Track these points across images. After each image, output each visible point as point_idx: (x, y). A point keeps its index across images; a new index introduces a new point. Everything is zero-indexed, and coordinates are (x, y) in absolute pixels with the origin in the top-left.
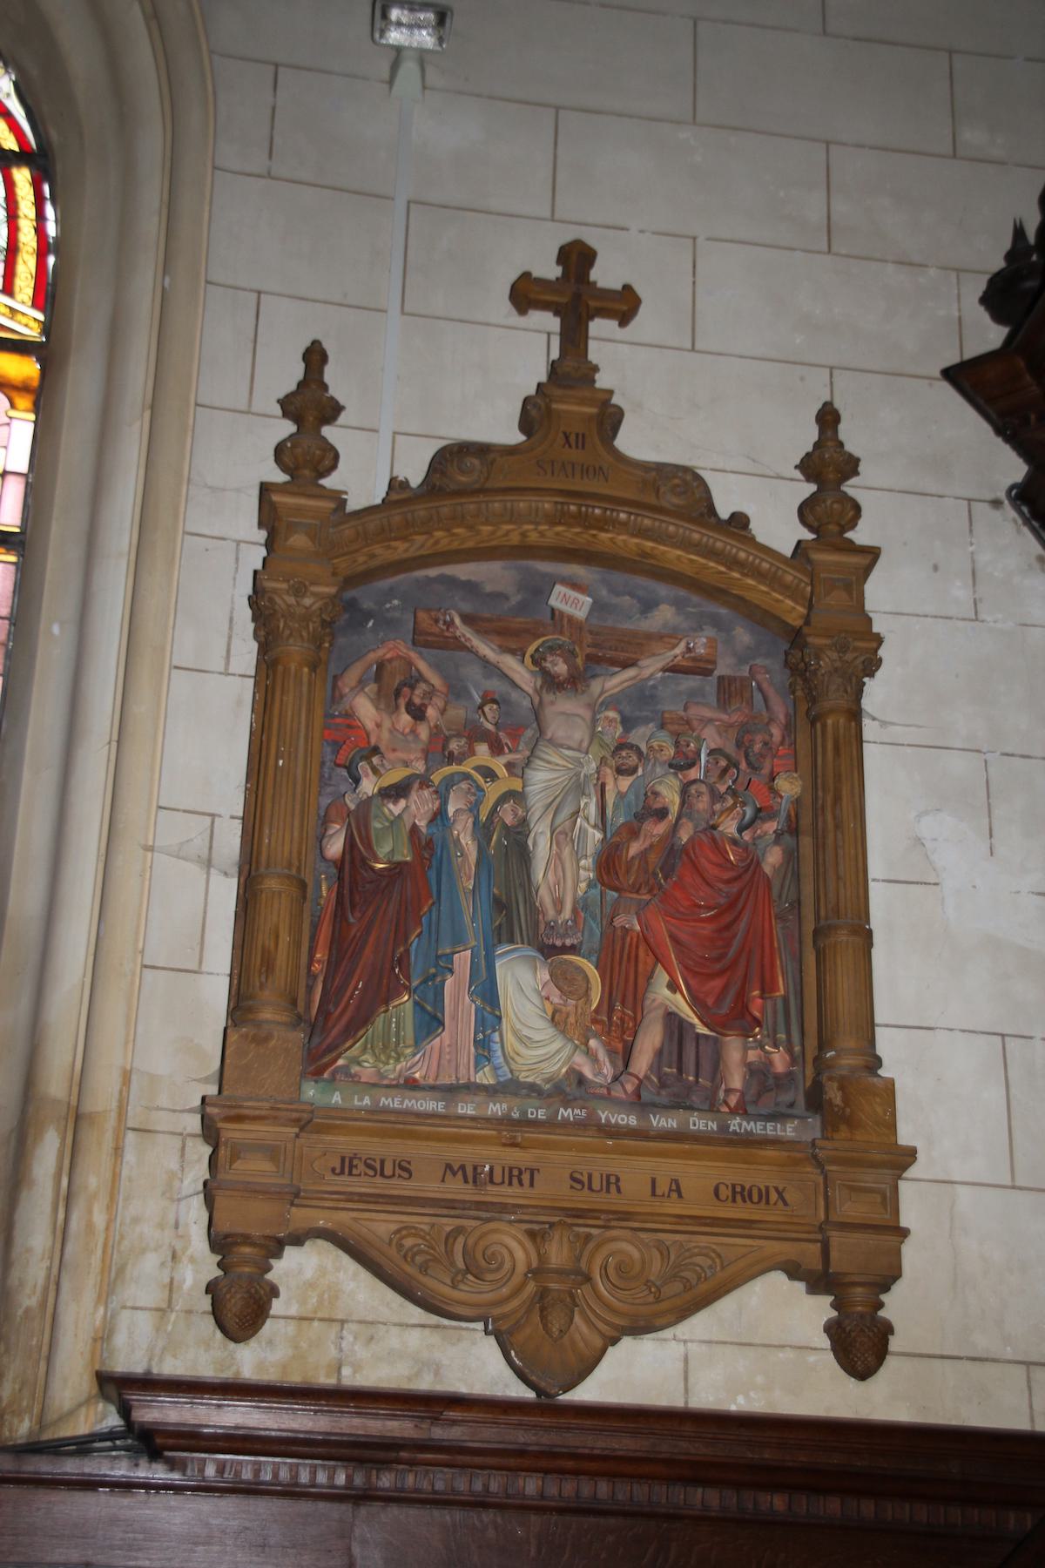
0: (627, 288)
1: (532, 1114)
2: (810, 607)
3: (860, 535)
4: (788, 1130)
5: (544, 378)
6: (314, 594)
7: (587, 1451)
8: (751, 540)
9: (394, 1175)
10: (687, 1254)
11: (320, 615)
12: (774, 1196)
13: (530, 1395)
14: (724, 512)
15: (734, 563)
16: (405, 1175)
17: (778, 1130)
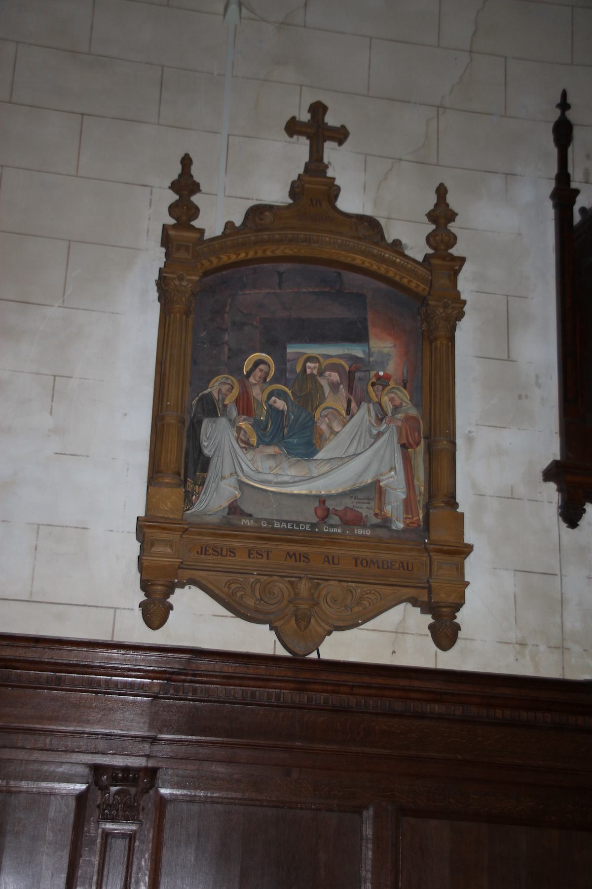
0: (343, 127)
1: (302, 527)
2: (431, 287)
3: (455, 251)
5: (301, 170)
9: (226, 556)
13: (287, 654)
14: (390, 240)
15: (394, 264)
16: (233, 555)
17: (295, 526)
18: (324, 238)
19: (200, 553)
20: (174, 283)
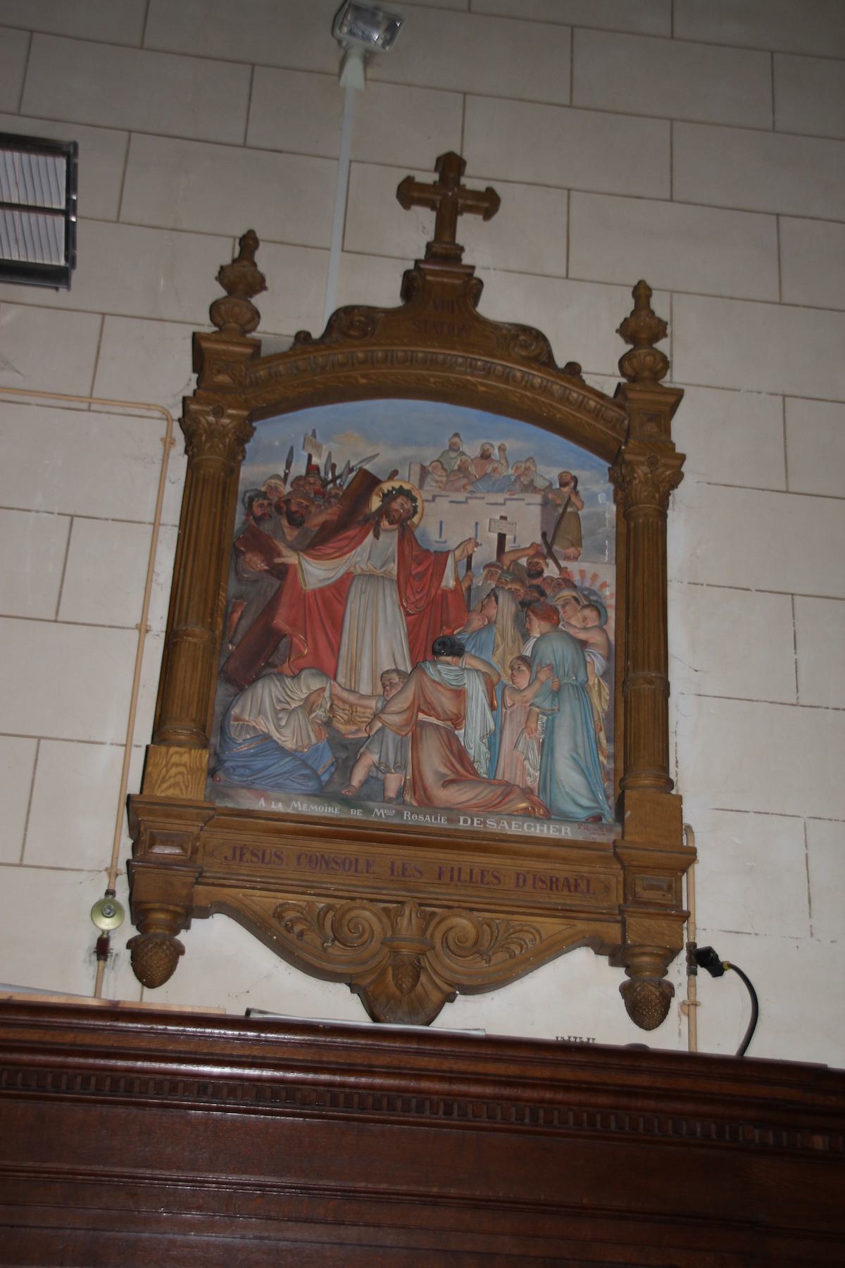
1: (465, 821)
4: (513, 826)
6: (230, 416)
7: (92, 1027)
8: (582, 384)
9: (270, 862)
10: (512, 931)
11: (235, 432)
12: (583, 886)
14: (561, 362)
18: (531, 377)
19: (229, 859)
20: (206, 420)
